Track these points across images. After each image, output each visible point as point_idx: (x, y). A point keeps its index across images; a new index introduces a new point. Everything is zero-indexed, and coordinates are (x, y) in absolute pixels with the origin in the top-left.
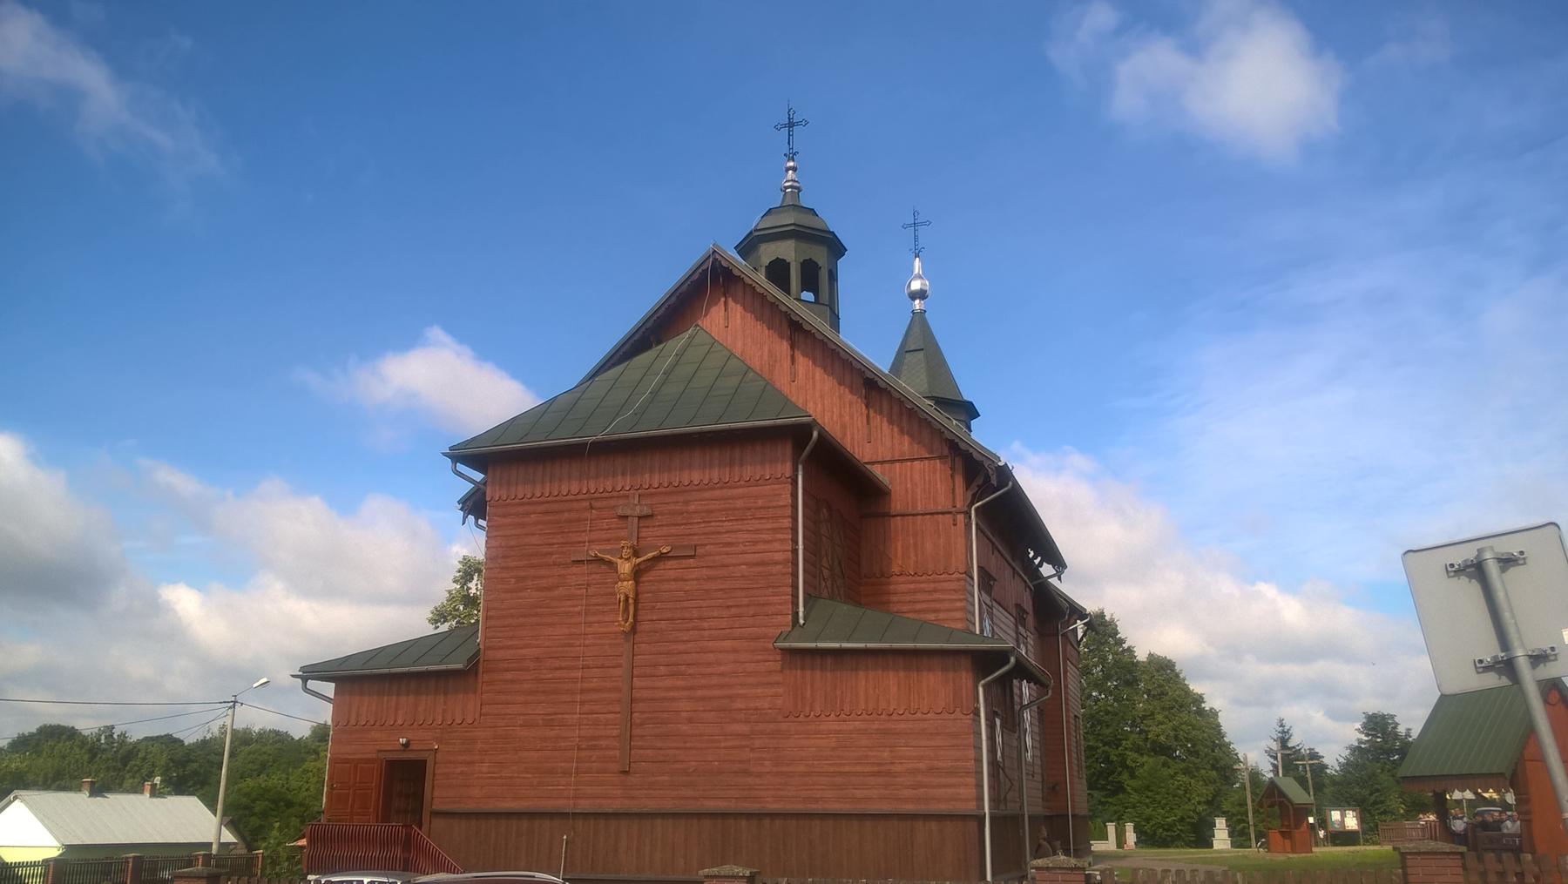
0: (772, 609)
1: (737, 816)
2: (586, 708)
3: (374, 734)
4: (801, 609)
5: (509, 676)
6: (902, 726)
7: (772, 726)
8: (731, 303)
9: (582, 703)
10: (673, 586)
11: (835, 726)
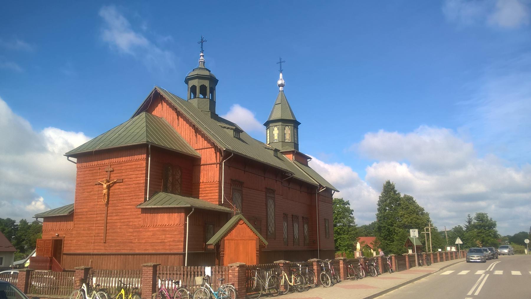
0: (140, 197)
1: (129, 254)
2: (97, 225)
3: (51, 233)
4: (148, 196)
5: (80, 216)
6: (168, 229)
7: (137, 230)
8: (163, 103)
9: (96, 224)
10: (117, 190)
11: (152, 229)
